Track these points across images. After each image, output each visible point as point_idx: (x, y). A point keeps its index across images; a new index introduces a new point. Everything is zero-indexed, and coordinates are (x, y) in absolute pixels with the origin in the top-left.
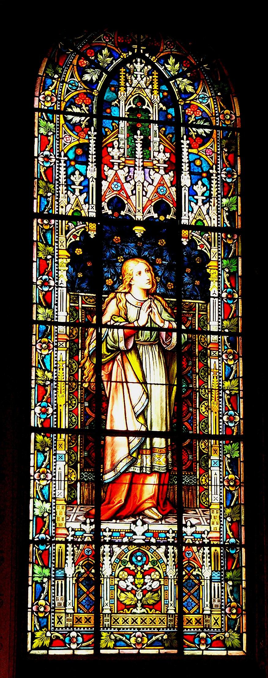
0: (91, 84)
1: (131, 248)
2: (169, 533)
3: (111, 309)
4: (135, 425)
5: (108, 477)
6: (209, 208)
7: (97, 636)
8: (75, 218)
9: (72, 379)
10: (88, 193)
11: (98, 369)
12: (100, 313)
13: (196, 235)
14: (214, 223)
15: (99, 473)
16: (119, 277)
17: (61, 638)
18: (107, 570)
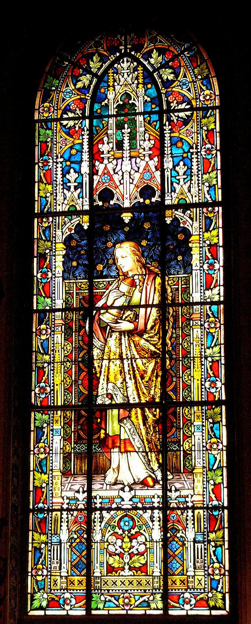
6: (190, 186)
7: (89, 597)
10: (82, 187)
13: (179, 213)
14: (196, 200)
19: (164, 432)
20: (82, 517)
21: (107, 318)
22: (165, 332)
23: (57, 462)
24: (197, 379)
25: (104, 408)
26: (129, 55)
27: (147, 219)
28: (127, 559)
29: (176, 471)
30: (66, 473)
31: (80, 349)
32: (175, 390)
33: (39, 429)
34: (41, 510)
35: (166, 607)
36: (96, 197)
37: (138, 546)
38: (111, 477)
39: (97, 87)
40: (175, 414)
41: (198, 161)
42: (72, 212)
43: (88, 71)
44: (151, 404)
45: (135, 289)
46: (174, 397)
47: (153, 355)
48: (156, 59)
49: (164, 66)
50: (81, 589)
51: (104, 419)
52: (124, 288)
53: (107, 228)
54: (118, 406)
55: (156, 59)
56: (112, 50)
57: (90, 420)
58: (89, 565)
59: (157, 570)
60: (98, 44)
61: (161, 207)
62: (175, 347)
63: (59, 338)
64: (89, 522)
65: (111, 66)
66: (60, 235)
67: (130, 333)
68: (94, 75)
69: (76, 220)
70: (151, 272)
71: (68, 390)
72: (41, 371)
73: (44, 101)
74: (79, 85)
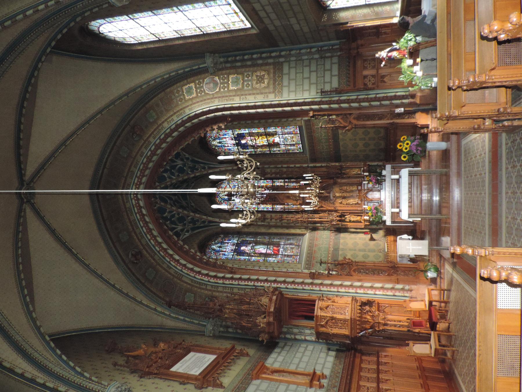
0: (214, 252)
1: (239, 249)
2: (190, 167)
3: (247, 252)
4: (266, 250)
5: (273, 253)
7: (298, 144)
8: (233, 255)
9: (257, 257)
11: (256, 253)
12: (248, 253)
15: (272, 254)
16: (243, 250)
17: (236, 89)
18: (287, 254)
19: (271, 135)
21: (254, 144)
23: (278, 149)
24: (347, 3)
30: (280, 148)
38: (279, 142)
44: (266, 137)
46: (342, 125)
47: (258, 137)
50: (297, 145)
52: (248, 141)
55: (210, 139)
59: (293, 135)
61: (234, 137)
63: (258, 150)
64: (287, 144)
66: (242, 150)
67: (256, 140)
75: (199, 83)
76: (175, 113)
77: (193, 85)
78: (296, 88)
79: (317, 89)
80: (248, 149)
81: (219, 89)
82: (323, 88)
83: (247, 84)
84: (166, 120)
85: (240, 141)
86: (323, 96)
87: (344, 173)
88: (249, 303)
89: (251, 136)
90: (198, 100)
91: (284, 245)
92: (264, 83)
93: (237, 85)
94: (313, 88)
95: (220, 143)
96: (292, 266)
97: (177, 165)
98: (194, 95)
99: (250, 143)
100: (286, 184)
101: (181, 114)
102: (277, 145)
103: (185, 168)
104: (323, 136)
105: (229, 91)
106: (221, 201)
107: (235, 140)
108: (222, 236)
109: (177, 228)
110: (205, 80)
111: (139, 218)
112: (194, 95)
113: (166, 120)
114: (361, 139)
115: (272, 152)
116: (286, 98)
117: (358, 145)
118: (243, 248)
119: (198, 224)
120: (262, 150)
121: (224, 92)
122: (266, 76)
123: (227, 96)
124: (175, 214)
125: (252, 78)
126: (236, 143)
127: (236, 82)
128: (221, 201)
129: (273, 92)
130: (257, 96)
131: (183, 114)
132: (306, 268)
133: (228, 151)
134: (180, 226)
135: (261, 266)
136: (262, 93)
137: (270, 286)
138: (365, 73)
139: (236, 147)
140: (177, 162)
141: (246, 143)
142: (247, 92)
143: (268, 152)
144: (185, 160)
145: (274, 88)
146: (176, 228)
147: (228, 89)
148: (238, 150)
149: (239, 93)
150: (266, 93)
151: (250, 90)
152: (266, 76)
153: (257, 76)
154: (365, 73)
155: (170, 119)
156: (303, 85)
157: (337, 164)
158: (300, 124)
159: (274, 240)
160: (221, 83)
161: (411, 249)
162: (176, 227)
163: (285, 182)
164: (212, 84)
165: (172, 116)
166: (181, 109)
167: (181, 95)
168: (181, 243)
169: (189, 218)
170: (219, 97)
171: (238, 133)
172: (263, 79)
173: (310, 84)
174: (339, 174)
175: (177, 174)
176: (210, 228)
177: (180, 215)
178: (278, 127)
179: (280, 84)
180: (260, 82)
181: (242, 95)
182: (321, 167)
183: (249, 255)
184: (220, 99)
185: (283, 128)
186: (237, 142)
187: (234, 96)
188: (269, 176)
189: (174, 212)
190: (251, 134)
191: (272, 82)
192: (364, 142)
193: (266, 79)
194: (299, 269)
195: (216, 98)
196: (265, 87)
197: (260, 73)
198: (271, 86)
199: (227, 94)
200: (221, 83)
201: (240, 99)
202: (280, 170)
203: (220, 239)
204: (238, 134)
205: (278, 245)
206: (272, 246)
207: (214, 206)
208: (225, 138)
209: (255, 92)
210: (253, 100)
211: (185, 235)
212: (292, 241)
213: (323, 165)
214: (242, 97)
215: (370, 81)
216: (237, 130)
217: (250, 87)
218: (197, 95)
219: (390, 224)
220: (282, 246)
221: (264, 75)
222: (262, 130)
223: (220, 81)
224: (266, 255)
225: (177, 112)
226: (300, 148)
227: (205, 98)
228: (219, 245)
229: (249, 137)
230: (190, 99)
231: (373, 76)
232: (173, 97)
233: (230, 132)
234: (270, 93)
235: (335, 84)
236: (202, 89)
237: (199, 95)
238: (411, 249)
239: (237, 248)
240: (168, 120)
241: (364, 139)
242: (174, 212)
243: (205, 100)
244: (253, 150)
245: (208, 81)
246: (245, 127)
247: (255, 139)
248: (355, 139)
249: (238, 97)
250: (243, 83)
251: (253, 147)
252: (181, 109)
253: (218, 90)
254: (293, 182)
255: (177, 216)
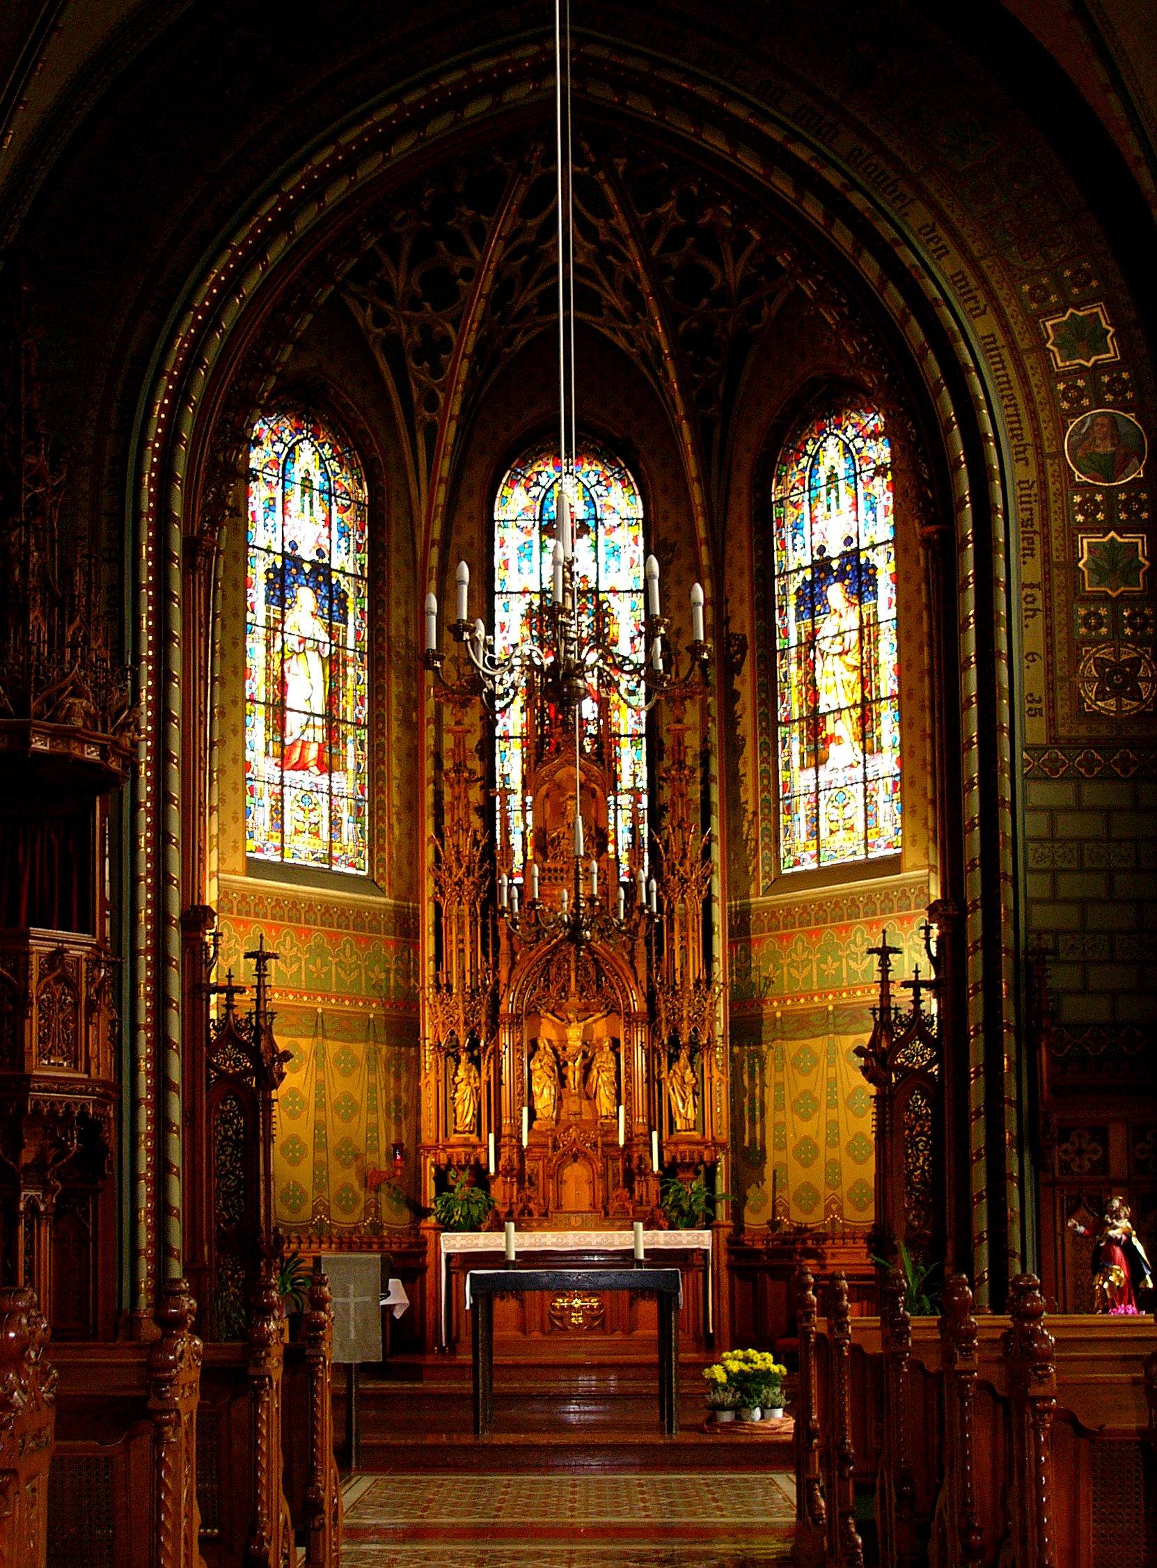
1: (302, 579)
11: (283, 662)
19: (863, 725)
20: (812, 799)
22: (862, 648)
25: (824, 715)
26: (832, 434)
27: (849, 562)
28: (841, 823)
29: (872, 752)
30: (802, 768)
31: (807, 674)
32: (870, 692)
33: (784, 739)
34: (787, 798)
35: (867, 853)
36: (815, 553)
37: (848, 812)
39: (812, 465)
40: (871, 710)
41: (556, 870)
42: (800, 568)
43: (806, 453)
44: (855, 706)
45: (1150, 1325)
48: (851, 432)
49: (857, 436)
51: (825, 722)
53: (822, 575)
54: (833, 712)
55: (851, 432)
56: (821, 432)
57: (816, 725)
58: (818, 832)
59: (860, 827)
60: (812, 431)
61: (857, 551)
62: (869, 659)
64: (817, 801)
65: (821, 446)
66: (792, 589)
67: (840, 654)
68: (810, 456)
69: (528, 597)
70: (852, 604)
71: (801, 707)
72: (783, 695)
73: (778, 484)
74: (801, 466)
75: (1117, 387)
76: (973, 264)
77: (1111, 354)
78: (1071, 840)
79: (1056, 933)
80: (799, 616)
81: (1084, 484)
82: (1063, 956)
83: (1099, 617)
84: (942, 219)
85: (841, 576)
86: (1022, 956)
87: (678, 1058)
88: (57, 642)
89: (861, 630)
90: (1034, 381)
91: (330, 794)
92: (1102, 695)
93: (1095, 568)
94: (1067, 917)
95: (832, 478)
96: (232, 829)
97: (721, 265)
98: (1060, 363)
99: (828, 627)
100: (625, 800)
101: (967, 295)
102: (817, 758)
103: (705, 301)
104: (853, 964)
105: (1072, 532)
106: (537, 484)
107: (844, 555)
108: (363, 494)
109: (397, 267)
110: (1131, 416)
111: (446, 81)
112: (1060, 363)
113: (942, 219)
114: (833, 1125)
115: (782, 731)
116: (1025, 799)
117: (806, 1118)
118: (305, 598)
119: (418, 371)
120: (794, 682)
121: (1068, 510)
122: (1129, 705)
123: (1045, 522)
124: (471, 255)
125: (1128, 639)
126: (830, 559)
127: (1113, 564)
128: (537, 484)
129: (1054, 740)
130: (1040, 665)
131: (972, 304)
132: (224, 893)
133: (789, 521)
134: (408, 283)
135: (223, 684)
136: (1050, 687)
137: (139, 732)
138: (1117, 1137)
139: (807, 561)
140: (736, 259)
141: (827, 609)
142: (1059, 618)
143: (781, 715)
144: (745, 302)
145: (1072, 744)
146: (397, 267)
147: (1083, 528)
148: (792, 567)
149: (1059, 579)
150: (1052, 705)
151: (1071, 629)
152: (1129, 705)
153: (1135, 664)
154: (1117, 1137)
155: (946, 240)
156: (1082, 870)
157: (719, 1028)
158: (908, 862)
159: (350, 747)
160: (1110, 493)
161: (360, 1299)
162: (404, 263)
163: (634, 792)
164: (1110, 449)
165: (963, 249)
166: (991, 296)
167: (1063, 294)
168: (323, 296)
169: (450, 328)
170: (1043, 486)
171: (875, 568)
172: (1118, 692)
173: (1083, 903)
174: (674, 1041)
175: (675, 261)
176: (404, 431)
177: (460, 282)
178: (901, 762)
179: (1089, 771)
180: (1104, 679)
181: (1048, 596)
182: (708, 958)
183: (275, 628)
184: (1035, 490)
185: (895, 783)
186: (835, 565)
187: (1047, 557)
188: (666, 718)
189: (478, 256)
190: (868, 631)
191: (1103, 731)
192: (821, 1141)
193: (1119, 705)
194: (221, 860)
195: (1041, 469)
196: (1081, 700)
197: (1146, 679)
198: (1083, 731)
199: (1055, 525)
200: (1110, 493)
201: (1032, 586)
202: (693, 771)
203: (346, 481)
204: (870, 569)
205: (327, 766)
206: (320, 735)
207: (594, 1302)
208: (855, 505)
209: (1061, 655)
210: (1021, 647)
211: (364, 305)
212: (348, 828)
213: (718, 968)
214: (1038, 594)
215: (1080, 1152)
216: (891, 568)
217: (1083, 630)
218: (1060, 377)
219: (444, 1250)
220: (323, 780)
221: (1136, 695)
222: (887, 682)
223: (1120, 489)
224: (278, 710)
225: (983, 280)
226: (797, 863)
227: (1043, 416)
228: (317, 480)
229: (856, 625)
230: (1041, 341)
231: (1102, 1165)
232: (1056, 254)
233: (883, 529)
234: (1052, 724)
235: (1074, 1009)
236: (1085, 402)
237: (1061, 386)
238: (360, 1299)
239: (307, 568)
240: (940, 231)
241: (832, 1144)
242: (478, 256)
243: (1033, 415)
244: (793, 641)
245: (1123, 429)
246: (903, 605)
247: (845, 653)
248: (832, 1105)
249: (1037, 578)
250: (1105, 599)
251: (810, 641)
252: (991, 296)
253: (1079, 477)
254: (634, 831)
255: (458, 264)
